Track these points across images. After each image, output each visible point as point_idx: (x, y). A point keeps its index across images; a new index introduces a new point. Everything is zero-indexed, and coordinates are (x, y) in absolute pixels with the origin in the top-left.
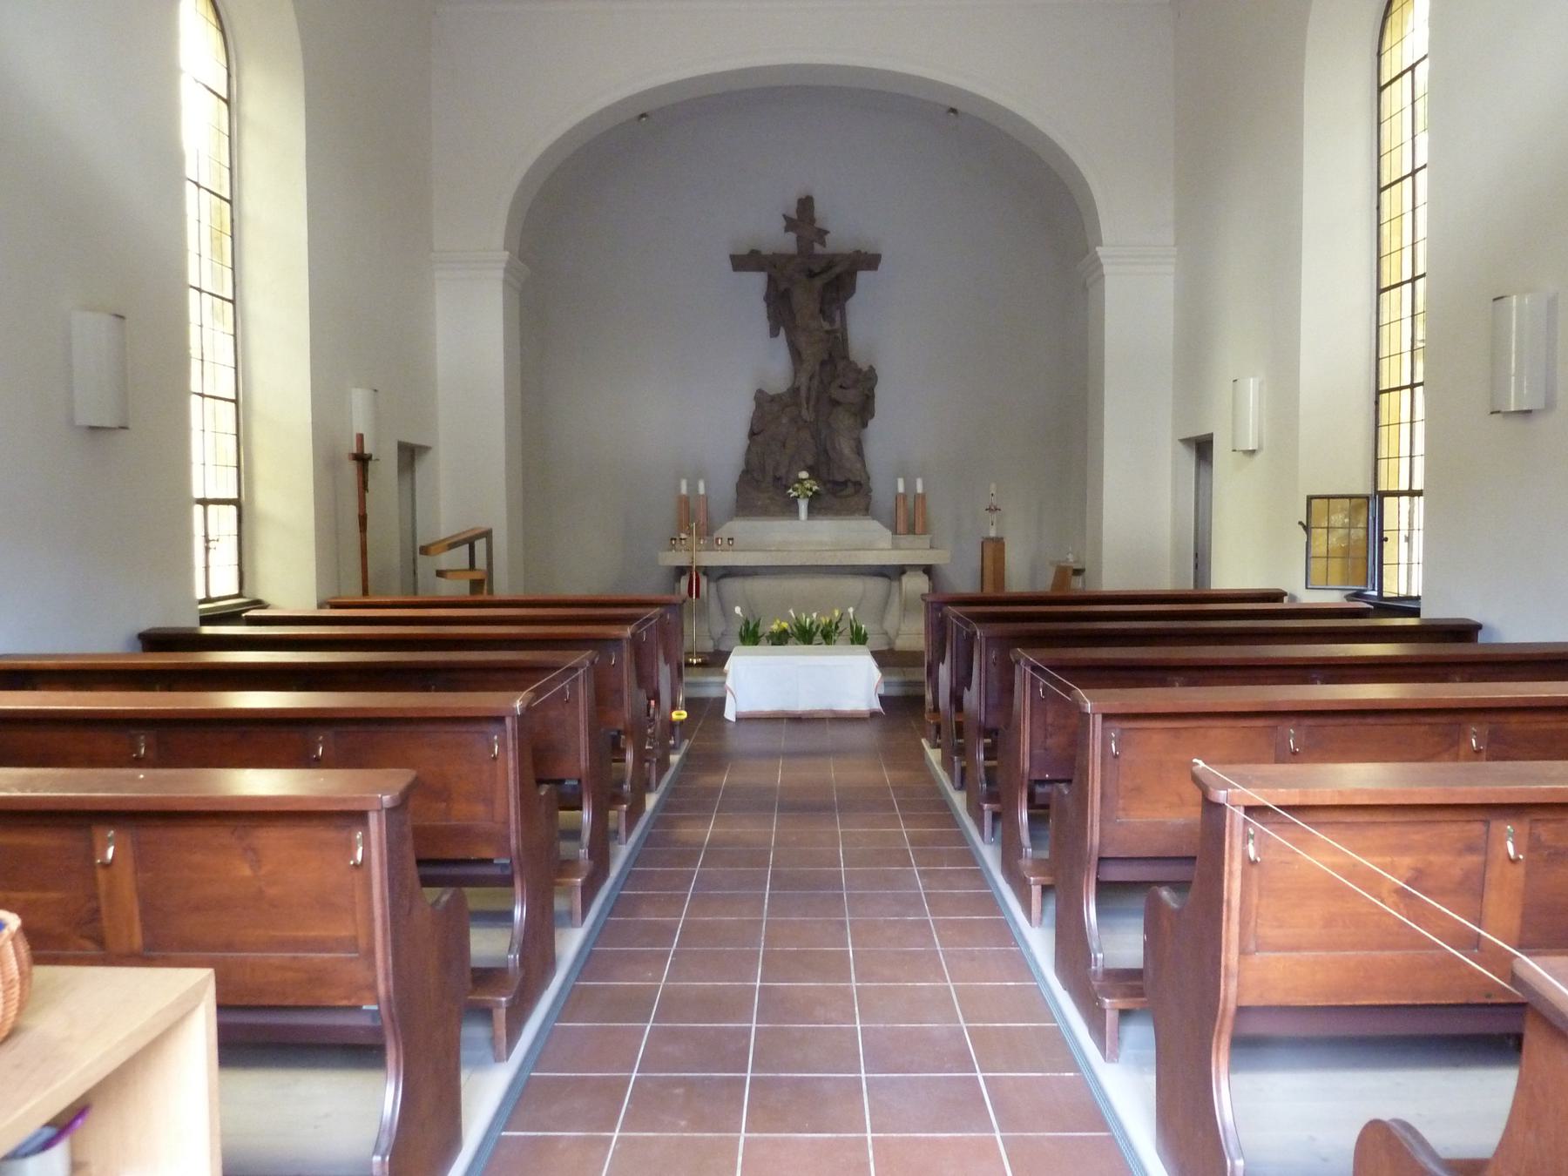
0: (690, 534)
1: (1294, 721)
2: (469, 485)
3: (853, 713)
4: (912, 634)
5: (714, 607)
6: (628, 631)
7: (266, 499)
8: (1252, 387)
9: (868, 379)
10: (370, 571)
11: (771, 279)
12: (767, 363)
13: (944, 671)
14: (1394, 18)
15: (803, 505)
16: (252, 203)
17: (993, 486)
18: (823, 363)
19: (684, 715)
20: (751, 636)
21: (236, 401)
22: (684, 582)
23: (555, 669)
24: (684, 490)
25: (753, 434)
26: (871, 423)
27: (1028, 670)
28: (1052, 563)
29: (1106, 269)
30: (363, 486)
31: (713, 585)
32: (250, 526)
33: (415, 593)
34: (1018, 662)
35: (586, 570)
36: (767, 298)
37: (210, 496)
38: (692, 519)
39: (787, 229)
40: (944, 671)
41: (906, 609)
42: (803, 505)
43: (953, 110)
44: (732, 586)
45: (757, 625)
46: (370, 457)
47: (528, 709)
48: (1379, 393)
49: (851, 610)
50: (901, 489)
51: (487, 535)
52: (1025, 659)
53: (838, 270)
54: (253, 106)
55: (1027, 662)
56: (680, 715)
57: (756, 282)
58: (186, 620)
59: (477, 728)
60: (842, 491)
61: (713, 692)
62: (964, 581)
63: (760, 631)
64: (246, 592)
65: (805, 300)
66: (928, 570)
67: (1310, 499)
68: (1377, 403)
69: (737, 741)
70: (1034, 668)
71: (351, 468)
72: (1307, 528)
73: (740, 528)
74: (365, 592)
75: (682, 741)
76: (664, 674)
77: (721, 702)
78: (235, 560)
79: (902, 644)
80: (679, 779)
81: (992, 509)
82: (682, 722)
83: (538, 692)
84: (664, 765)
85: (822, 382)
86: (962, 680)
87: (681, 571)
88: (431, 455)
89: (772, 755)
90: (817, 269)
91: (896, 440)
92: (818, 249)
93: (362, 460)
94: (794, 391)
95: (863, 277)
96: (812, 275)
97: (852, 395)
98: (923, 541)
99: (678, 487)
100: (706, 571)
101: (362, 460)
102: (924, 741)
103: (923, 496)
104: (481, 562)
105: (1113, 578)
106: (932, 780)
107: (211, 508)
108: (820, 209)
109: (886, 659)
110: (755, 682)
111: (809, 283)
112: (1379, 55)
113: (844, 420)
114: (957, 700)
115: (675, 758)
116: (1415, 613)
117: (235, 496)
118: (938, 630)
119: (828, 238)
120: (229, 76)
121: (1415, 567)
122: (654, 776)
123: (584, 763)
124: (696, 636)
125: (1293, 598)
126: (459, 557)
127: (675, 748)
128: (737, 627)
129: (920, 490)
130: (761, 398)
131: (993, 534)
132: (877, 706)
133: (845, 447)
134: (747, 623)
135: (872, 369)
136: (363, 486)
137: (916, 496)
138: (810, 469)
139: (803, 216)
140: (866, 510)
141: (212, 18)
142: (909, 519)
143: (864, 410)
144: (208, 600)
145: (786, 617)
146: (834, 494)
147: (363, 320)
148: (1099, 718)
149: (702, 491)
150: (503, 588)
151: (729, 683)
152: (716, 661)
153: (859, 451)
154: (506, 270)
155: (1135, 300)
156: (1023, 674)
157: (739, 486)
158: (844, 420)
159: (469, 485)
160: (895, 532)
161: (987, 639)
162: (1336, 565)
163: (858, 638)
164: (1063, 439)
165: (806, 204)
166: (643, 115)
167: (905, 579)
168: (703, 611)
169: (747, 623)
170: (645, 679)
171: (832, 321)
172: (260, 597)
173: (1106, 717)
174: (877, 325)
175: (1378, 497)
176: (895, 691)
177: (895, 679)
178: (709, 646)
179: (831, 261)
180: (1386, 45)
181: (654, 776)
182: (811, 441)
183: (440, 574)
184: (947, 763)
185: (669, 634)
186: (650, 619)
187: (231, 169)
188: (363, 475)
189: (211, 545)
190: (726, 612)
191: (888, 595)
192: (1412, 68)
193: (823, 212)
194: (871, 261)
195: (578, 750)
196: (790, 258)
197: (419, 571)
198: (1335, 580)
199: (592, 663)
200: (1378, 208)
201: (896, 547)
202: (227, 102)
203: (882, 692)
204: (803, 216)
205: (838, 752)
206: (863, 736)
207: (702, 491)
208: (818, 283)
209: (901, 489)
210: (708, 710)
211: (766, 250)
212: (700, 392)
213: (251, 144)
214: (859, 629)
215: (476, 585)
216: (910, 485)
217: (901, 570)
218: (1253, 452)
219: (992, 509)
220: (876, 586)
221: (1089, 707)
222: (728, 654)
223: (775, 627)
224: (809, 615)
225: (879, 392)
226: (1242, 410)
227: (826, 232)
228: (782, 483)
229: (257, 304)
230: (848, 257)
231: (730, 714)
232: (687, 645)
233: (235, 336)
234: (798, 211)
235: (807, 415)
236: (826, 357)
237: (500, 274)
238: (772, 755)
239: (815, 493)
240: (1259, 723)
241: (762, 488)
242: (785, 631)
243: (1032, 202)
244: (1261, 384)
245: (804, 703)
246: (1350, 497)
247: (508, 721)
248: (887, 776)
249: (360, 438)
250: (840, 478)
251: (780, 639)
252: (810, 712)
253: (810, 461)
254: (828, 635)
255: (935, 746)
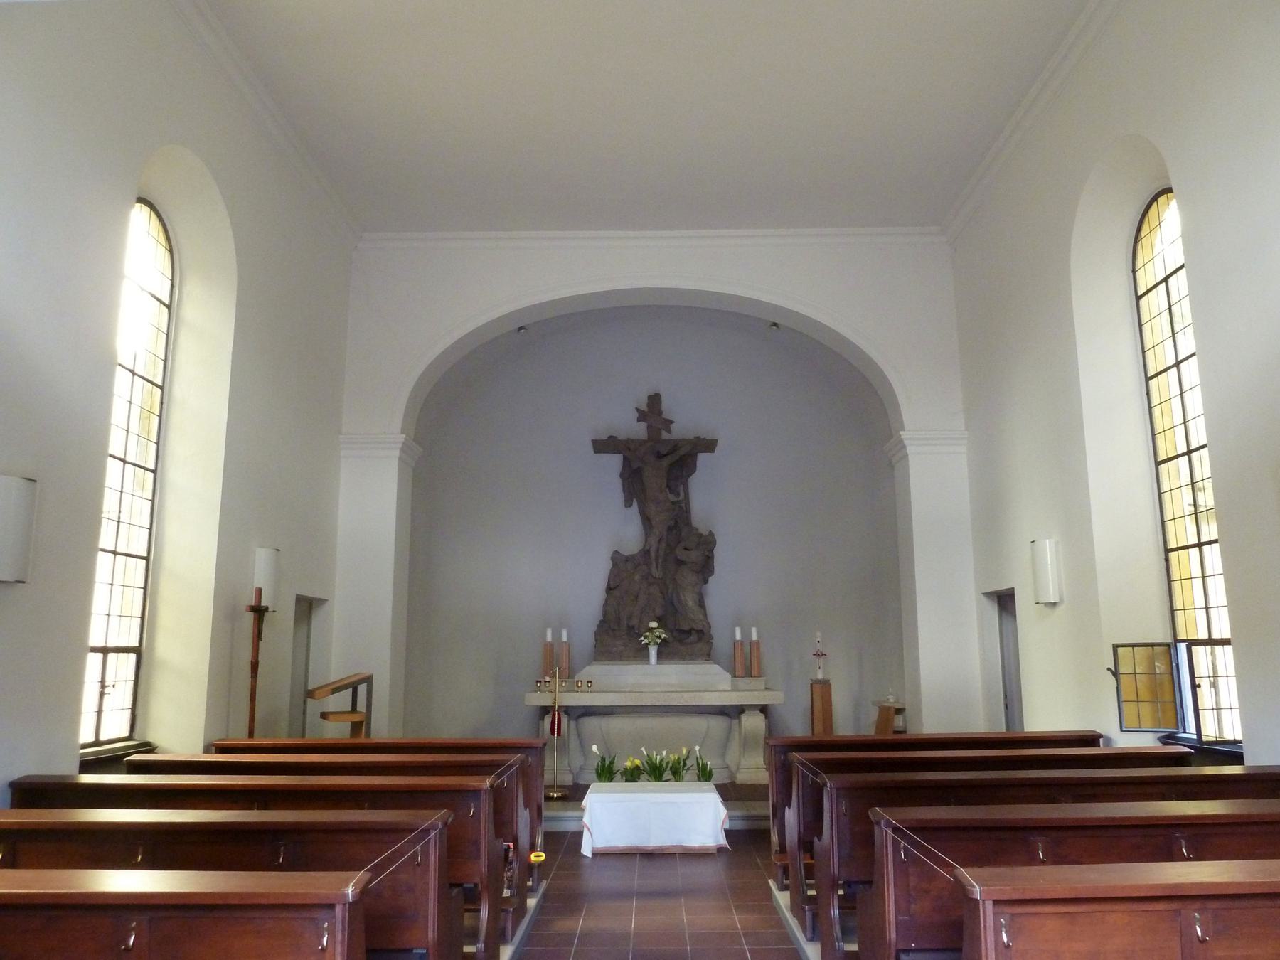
0: (553, 676)
1: (1198, 905)
2: (359, 633)
3: (701, 848)
4: (754, 769)
5: (574, 743)
6: (486, 783)
7: (166, 648)
8: (1049, 549)
9: (707, 544)
10: (257, 716)
11: (626, 460)
12: (624, 530)
13: (791, 815)
14: (1144, 243)
15: (653, 651)
16: (180, 390)
17: (819, 634)
18: (670, 529)
19: (543, 856)
20: (606, 773)
21: (147, 559)
22: (548, 720)
23: (413, 831)
24: (549, 638)
25: (609, 589)
26: (711, 579)
27: (890, 832)
28: (873, 704)
29: (909, 450)
30: (258, 635)
31: (573, 723)
32: (140, 670)
33: (303, 736)
34: (878, 823)
35: (459, 714)
36: (621, 475)
37: (112, 643)
38: (555, 664)
39: (639, 420)
40: (791, 815)
41: (746, 743)
42: (653, 651)
43: (775, 324)
44: (590, 723)
45: (612, 763)
46: (266, 609)
47: (363, 893)
48: (1167, 551)
49: (697, 748)
50: (738, 637)
51: (368, 680)
52: (885, 819)
53: (682, 452)
54: (191, 311)
55: (889, 824)
56: (538, 857)
57: (614, 462)
58: (64, 767)
59: (306, 914)
60: (687, 639)
61: (571, 827)
62: (797, 726)
63: (615, 769)
64: (136, 735)
65: (654, 478)
66: (764, 709)
67: (1116, 647)
68: (1167, 560)
69: (594, 880)
70: (895, 830)
71: (249, 618)
72: (1116, 674)
73: (598, 671)
74: (251, 734)
75: (540, 880)
76: (523, 817)
77: (579, 835)
78: (129, 704)
79: (743, 777)
80: (535, 924)
81: (819, 655)
82: (540, 864)
83: (376, 871)
84: (521, 910)
85: (668, 545)
86: (812, 824)
87: (545, 710)
88: (326, 607)
89: (625, 895)
90: (664, 450)
91: (736, 592)
92: (665, 436)
93: (259, 612)
94: (645, 553)
95: (702, 458)
96: (660, 456)
97: (694, 556)
98: (759, 683)
99: (545, 635)
100: (568, 710)
101: (259, 612)
102: (770, 881)
103: (758, 642)
104: (361, 706)
105: (931, 724)
106: (780, 923)
107: (111, 656)
108: (666, 404)
109: (730, 793)
110: (612, 818)
111: (658, 464)
112: (1134, 271)
113: (687, 578)
114: (806, 845)
115: (532, 902)
116: (1237, 758)
117: (136, 644)
118: (783, 772)
119: (673, 426)
120: (172, 286)
121: (1225, 714)
122: (510, 925)
123: (431, 935)
124: (556, 770)
125: (1109, 741)
126: (340, 701)
127: (532, 890)
128: (595, 763)
129: (755, 637)
130: (618, 560)
131: (820, 676)
132: (723, 841)
133: (690, 601)
134: (603, 760)
135: (711, 534)
136: (258, 635)
137: (751, 643)
138: (658, 619)
139: (652, 410)
140: (708, 656)
141: (163, 240)
142: (745, 664)
143: (705, 568)
144: (97, 743)
145: (638, 754)
146: (680, 641)
147: (271, 487)
148: (989, 905)
149: (565, 639)
150: (382, 730)
151: (586, 820)
152: (574, 794)
153: (702, 604)
154: (402, 450)
155: (935, 475)
156: (885, 836)
157: (596, 634)
158: (687, 578)
159: (359, 633)
160: (734, 676)
161: (837, 789)
162: (1146, 709)
163: (704, 774)
164: (880, 593)
165: (655, 400)
166: (521, 328)
167: (744, 717)
168: (563, 749)
169: (603, 760)
170: (503, 826)
171: (678, 494)
172: (150, 739)
173: (996, 902)
174: (713, 497)
175: (1169, 649)
176: (739, 825)
177: (738, 813)
178: (568, 780)
179: (675, 445)
180: (1139, 263)
181: (510, 925)
182: (658, 597)
183: (324, 716)
184: (796, 908)
185: (529, 774)
186: (511, 766)
187: (165, 361)
188: (252, 624)
189: (106, 690)
190: (584, 748)
191: (730, 731)
192: (1166, 280)
193: (669, 407)
194: (709, 446)
195: (426, 917)
196: (642, 443)
197: (308, 711)
198: (1147, 723)
199: (445, 824)
200: (1148, 394)
201: (735, 689)
202: (169, 307)
203: (727, 827)
204: (652, 410)
205: (688, 892)
206: (712, 873)
207: (565, 639)
208: (665, 463)
209: (738, 637)
210: (565, 844)
211: (622, 436)
212: (564, 555)
213: (186, 343)
214: (705, 766)
215: (356, 727)
216: (746, 634)
217: (739, 710)
218: (1054, 604)
219: (819, 655)
220: (718, 723)
221: (977, 892)
222: (586, 787)
223: (628, 764)
224: (659, 753)
225: (718, 552)
226: (1041, 568)
227: (672, 422)
228: (634, 632)
229: (175, 473)
230: (689, 441)
231: (586, 850)
232: (548, 777)
233: (153, 501)
234: (648, 405)
235: (656, 572)
236: (672, 523)
237: (397, 453)
238: (625, 895)
239: (664, 640)
240: (1161, 906)
241: (617, 635)
242: (637, 768)
243: (844, 399)
244: (1057, 543)
245: (656, 839)
246: (1152, 645)
247: (338, 909)
248: (737, 920)
249: (259, 591)
250: (686, 628)
251: (633, 775)
252: (661, 848)
253: (659, 612)
254: (677, 772)
255: (783, 888)
